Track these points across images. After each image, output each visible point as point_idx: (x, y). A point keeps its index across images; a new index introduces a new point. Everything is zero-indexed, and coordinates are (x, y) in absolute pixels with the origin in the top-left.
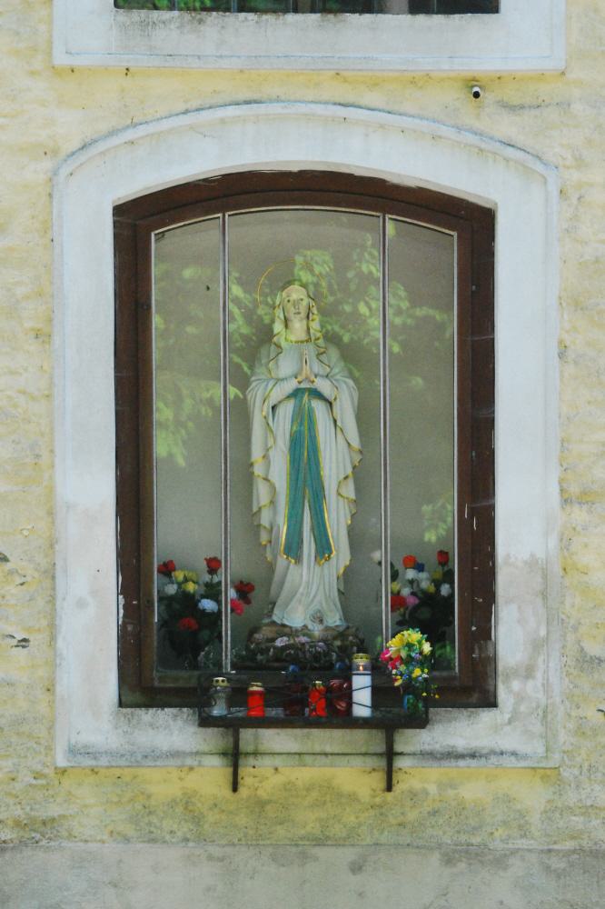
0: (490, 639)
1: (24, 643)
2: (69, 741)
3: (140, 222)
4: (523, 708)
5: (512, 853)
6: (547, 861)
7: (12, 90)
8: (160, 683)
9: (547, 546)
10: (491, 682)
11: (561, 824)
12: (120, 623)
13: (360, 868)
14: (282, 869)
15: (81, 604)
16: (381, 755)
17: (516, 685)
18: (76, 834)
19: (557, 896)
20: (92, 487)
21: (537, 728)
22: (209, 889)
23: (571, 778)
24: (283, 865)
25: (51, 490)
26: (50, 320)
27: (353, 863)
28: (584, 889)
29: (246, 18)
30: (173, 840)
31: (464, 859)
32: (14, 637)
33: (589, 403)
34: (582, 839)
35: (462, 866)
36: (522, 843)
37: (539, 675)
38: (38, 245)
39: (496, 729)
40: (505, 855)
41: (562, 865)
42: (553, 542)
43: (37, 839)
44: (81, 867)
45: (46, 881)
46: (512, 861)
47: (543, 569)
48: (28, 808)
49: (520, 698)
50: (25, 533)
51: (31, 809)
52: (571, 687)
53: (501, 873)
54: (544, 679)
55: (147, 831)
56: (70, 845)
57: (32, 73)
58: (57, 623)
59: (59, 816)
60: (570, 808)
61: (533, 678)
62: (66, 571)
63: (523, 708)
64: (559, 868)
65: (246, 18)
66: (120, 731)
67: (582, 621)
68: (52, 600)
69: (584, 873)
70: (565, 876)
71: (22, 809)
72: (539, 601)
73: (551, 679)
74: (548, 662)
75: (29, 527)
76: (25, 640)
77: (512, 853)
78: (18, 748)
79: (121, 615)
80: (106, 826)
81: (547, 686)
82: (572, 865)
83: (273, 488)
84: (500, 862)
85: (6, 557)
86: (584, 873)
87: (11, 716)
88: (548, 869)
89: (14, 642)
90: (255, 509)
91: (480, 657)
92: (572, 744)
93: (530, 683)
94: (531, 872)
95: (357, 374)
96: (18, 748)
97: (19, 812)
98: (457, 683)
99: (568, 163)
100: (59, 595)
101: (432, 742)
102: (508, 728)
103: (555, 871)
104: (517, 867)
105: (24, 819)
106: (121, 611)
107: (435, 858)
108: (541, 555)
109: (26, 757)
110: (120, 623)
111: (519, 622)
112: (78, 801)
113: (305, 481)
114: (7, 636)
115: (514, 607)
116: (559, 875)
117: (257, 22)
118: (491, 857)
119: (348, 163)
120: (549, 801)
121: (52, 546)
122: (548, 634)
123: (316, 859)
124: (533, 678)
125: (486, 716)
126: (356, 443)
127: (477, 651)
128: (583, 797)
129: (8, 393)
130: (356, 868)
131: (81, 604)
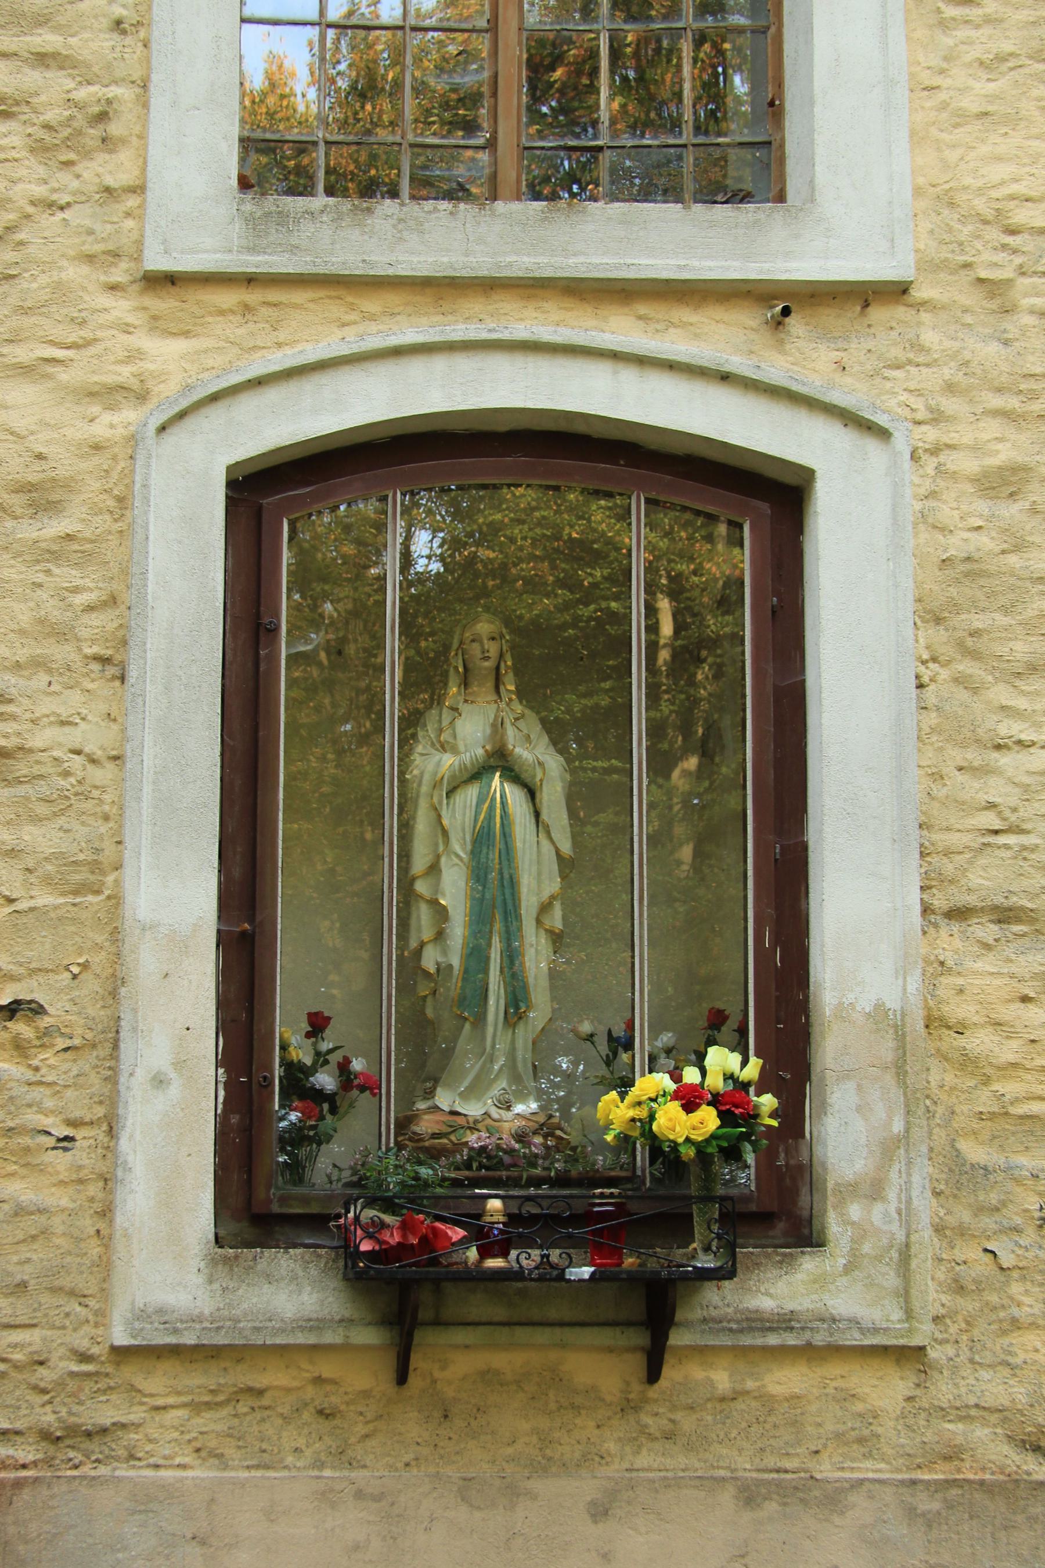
0: (803, 1136)
1: (65, 1144)
2: (133, 1303)
3: (261, 493)
4: (866, 1248)
5: (852, 1487)
6: (910, 1500)
7: (80, 311)
8: (280, 1206)
9: (905, 989)
10: (804, 1200)
11: (929, 1437)
12: (219, 1111)
13: (606, 1513)
14: (478, 1515)
15: (159, 1081)
16: (643, 1349)
17: (855, 1211)
18: (140, 1455)
19: (927, 1558)
20: (176, 894)
21: (891, 1280)
22: (357, 1548)
23: (944, 1361)
24: (479, 1508)
25: (116, 900)
26: (124, 643)
27: (593, 1503)
28: (972, 1546)
29: (435, 208)
30: (298, 1464)
31: (775, 1496)
32: (49, 1133)
33: (960, 769)
34: (962, 1460)
35: (772, 1507)
36: (869, 1469)
37: (892, 1195)
38: (110, 532)
39: (821, 1281)
40: (843, 1490)
41: (936, 1506)
42: (914, 983)
43: (76, 1461)
44: (146, 1511)
45: (90, 1535)
46: (853, 1498)
47: (896, 1026)
48: (64, 1411)
49: (862, 1232)
50: (75, 970)
51: (70, 1413)
52: (942, 1213)
53: (837, 1520)
54: (900, 1202)
55: (256, 1449)
56: (132, 1473)
57: (113, 288)
58: (121, 1111)
59: (114, 1424)
60: (942, 1409)
61: (884, 1199)
62: (135, 1029)
63: (866, 1248)
64: (929, 1512)
65: (435, 208)
66: (216, 1286)
67: (957, 1110)
68: (112, 1079)
69: (971, 1518)
70: (940, 1524)
71: (54, 1412)
72: (889, 1078)
73: (915, 1202)
74: (909, 1175)
75: (81, 961)
76: (67, 1139)
77: (852, 1487)
78: (52, 1313)
79: (221, 1099)
80: (189, 1441)
81: (906, 1214)
82: (950, 1506)
83: (441, 914)
84: (833, 1498)
85: (41, 1006)
86: (971, 1518)
87: (42, 1260)
88: (911, 1513)
89: (51, 1142)
90: (413, 944)
91: (787, 1165)
92: (943, 1305)
93: (878, 1209)
94: (885, 1517)
95: (837, 335)
96: (52, 1313)
97: (51, 1418)
98: (753, 1207)
99: (919, 416)
100: (125, 1067)
101: (720, 1304)
102: (844, 1281)
103: (923, 1515)
104: (861, 1509)
105: (57, 1429)
106: (222, 1093)
107: (727, 1497)
108: (893, 1003)
109: (64, 1328)
110: (219, 1111)
111: (859, 1109)
112: (145, 1400)
113: (42, 59)
114: (39, 1132)
115: (850, 1085)
116: (930, 1521)
117: (451, 213)
118: (816, 1493)
119: (617, 205)
120: (910, 1399)
121: (114, 994)
122: (907, 1130)
123: (534, 1497)
124: (884, 1199)
125: (809, 1264)
126: (566, 847)
127: (782, 1155)
128: (963, 1390)
129: (56, 753)
130: (599, 1512)
131: (159, 1081)
